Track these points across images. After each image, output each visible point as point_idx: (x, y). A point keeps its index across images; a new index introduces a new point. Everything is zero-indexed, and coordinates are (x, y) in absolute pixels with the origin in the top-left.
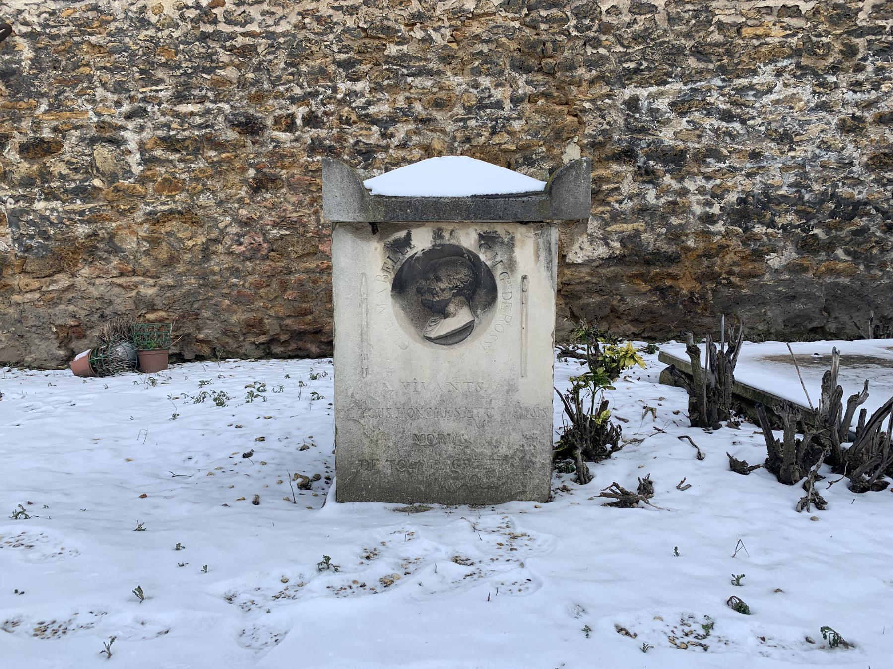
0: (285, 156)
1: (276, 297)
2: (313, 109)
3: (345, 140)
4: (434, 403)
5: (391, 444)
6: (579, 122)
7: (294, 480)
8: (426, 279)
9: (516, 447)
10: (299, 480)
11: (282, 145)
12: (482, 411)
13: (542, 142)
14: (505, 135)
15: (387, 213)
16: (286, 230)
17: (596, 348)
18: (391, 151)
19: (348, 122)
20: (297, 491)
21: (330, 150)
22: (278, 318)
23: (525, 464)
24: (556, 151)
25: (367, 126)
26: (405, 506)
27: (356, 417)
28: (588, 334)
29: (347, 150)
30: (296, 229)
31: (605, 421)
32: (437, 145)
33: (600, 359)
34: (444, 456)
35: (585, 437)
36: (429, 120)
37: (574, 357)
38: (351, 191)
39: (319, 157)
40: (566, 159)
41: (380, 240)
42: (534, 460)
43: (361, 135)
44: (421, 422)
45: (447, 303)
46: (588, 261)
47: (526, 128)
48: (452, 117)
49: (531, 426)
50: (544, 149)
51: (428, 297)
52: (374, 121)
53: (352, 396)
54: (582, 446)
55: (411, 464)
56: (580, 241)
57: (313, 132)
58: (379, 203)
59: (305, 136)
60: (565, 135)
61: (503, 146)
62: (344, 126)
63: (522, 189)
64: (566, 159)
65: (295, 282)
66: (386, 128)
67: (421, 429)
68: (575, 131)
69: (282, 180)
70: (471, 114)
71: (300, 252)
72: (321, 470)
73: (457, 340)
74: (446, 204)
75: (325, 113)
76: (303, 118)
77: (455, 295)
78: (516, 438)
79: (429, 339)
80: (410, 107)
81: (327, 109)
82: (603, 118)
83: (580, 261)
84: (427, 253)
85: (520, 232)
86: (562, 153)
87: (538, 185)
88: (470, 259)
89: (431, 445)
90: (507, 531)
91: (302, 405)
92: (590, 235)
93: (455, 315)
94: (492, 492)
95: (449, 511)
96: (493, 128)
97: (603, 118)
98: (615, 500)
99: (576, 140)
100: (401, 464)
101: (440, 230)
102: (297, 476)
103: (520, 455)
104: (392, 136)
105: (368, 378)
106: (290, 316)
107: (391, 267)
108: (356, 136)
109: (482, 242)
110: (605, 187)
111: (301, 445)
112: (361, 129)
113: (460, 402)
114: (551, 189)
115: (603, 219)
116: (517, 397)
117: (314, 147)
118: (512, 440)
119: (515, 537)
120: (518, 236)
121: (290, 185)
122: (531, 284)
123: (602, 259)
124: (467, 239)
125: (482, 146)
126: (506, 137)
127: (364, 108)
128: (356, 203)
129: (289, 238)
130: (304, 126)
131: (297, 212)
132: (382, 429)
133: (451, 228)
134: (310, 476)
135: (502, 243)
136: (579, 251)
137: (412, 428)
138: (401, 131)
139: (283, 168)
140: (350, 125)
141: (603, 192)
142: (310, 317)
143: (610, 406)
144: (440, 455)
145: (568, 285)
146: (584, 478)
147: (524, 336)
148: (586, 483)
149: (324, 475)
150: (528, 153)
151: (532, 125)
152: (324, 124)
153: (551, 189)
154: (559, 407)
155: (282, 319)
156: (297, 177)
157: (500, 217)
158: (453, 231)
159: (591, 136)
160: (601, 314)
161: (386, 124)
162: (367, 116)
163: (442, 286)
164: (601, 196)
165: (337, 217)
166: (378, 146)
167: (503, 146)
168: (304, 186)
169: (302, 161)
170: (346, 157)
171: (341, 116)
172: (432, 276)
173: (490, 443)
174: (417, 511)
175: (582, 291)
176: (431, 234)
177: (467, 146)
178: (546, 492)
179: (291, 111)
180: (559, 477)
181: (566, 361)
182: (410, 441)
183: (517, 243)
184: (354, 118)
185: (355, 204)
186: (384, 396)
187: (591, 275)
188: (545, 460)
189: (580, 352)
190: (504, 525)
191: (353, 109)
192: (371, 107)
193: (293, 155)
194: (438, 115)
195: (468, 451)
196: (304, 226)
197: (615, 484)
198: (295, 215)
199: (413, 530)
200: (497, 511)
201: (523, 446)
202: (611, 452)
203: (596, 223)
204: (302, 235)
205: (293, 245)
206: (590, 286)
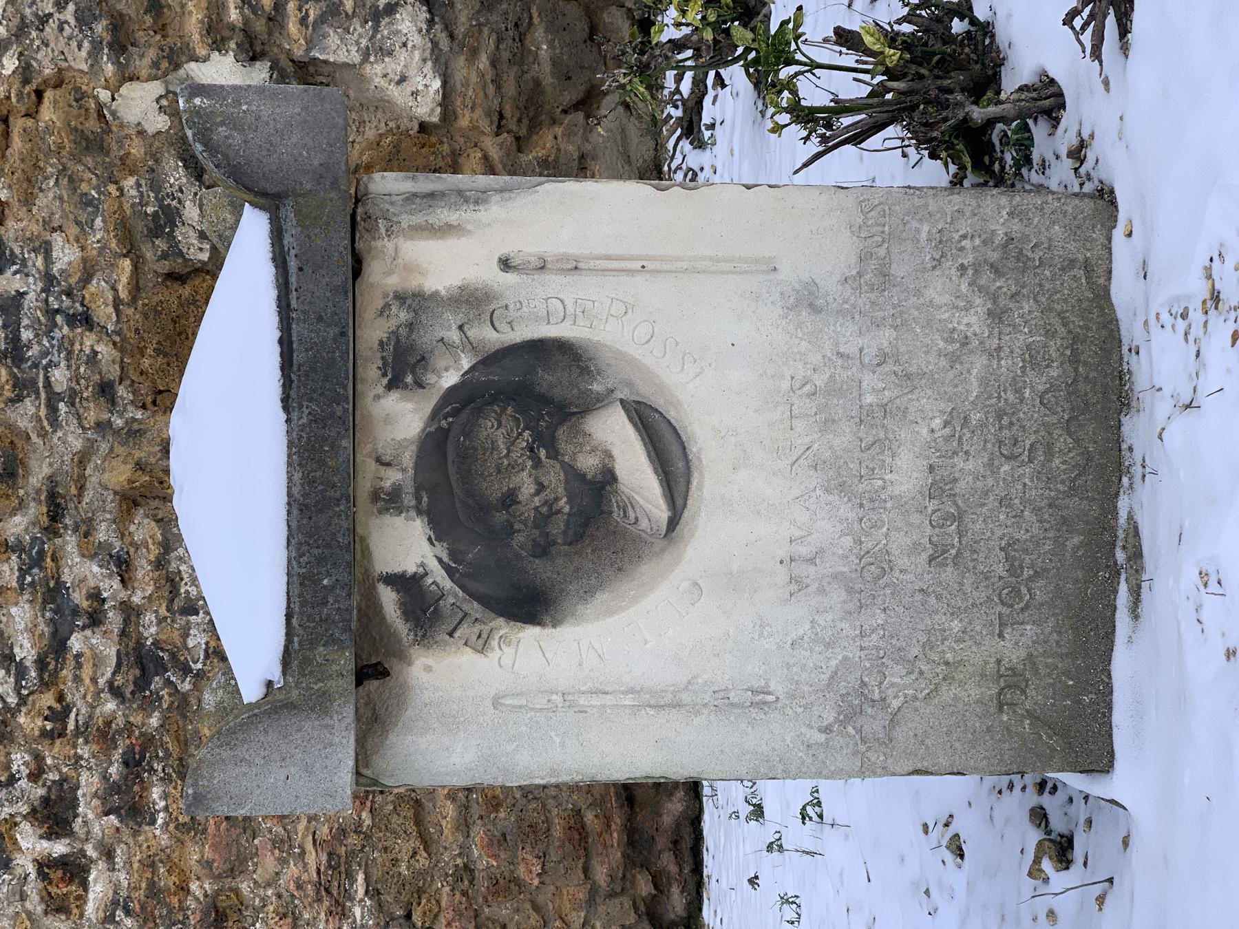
0: (152, 884)
1: (536, 907)
2: (25, 809)
3: (108, 724)
4: (846, 511)
5: (956, 625)
6: (57, 86)
7: (1046, 880)
8: (510, 530)
9: (964, 288)
10: (1047, 865)
11: (124, 893)
12: (868, 380)
13: (112, 188)
14: (93, 287)
15: (332, 640)
16: (351, 878)
17: (677, 45)
18: (137, 599)
19: (59, 715)
20: (1073, 876)
21: (133, 763)
22: (591, 901)
23: (1011, 263)
24: (137, 149)
25: (71, 663)
26: (1123, 588)
27: (882, 720)
28: (642, 70)
29: (136, 719)
30: (351, 854)
31: (892, 39)
32: (120, 475)
33: (708, 35)
34: (990, 481)
35: (933, 93)
36: (52, 496)
37: (699, 104)
38: (272, 737)
39: (156, 793)
40: (159, 123)
41: (402, 656)
42: (1000, 237)
43: (94, 680)
44: (899, 542)
45: (574, 476)
46: (436, 61)
47: (73, 230)
48: (43, 434)
49: (909, 246)
50: (129, 182)
51: (557, 528)
52: (58, 645)
53: (827, 730)
54: (959, 105)
55: (1011, 571)
56: (383, 83)
57: (87, 809)
58: (306, 661)
59: (96, 829)
60: (92, 125)
61: (123, 294)
62: (71, 726)
63: (267, 271)
64: (159, 123)
65: (496, 857)
66: (76, 612)
67: (916, 544)
68: (80, 96)
69: (217, 893)
70: (34, 382)
71: (414, 843)
72: (1018, 804)
73: (674, 448)
74: (309, 481)
75: (34, 777)
76: (50, 836)
77: (554, 454)
78: (940, 289)
79: (673, 523)
80: (18, 548)
81: (25, 771)
82: (44, 19)
83: (437, 84)
84: (440, 529)
85: (382, 277)
86: (141, 133)
87: (253, 229)
88: (455, 413)
89: (959, 518)
90: (1196, 316)
91: (831, 842)
92: (366, 54)
93: (608, 454)
94: (1088, 353)
95: (1137, 470)
96: (72, 320)
97: (44, 19)
98: (1111, 22)
99: (104, 95)
100: (1011, 598)
101: (375, 496)
102: (1035, 872)
103: (986, 277)
104: (95, 596)
105: (778, 687)
106: (586, 870)
107: (477, 628)
108: (98, 693)
109: (409, 379)
110: (234, 15)
111: (949, 857)
112: (77, 679)
113: (844, 438)
114: (264, 194)
115: (321, 20)
116: (830, 285)
117: (128, 805)
118: (946, 298)
119: (1216, 297)
120: (393, 282)
121: (232, 872)
122: (525, 245)
123: (431, 23)
124: (400, 420)
125: (122, 350)
126: (98, 285)
127: (21, 672)
128: (307, 725)
129: (376, 873)
130: (70, 834)
131: (303, 853)
132: (915, 651)
133: (372, 465)
134: (1033, 836)
135: (411, 326)
136: (408, 88)
137: (912, 569)
138: (82, 572)
139: (184, 889)
140: (67, 710)
141: (246, 21)
142: (589, 817)
143: (853, 24)
144: (986, 494)
145: (501, 117)
146: (1047, 99)
147: (666, 267)
148: (1061, 95)
149: (1032, 799)
150: (140, 227)
151: (65, 216)
152: (64, 779)
153: (264, 194)
154: (847, 164)
155: (593, 892)
156: (208, 853)
157: (343, 334)
158: (379, 461)
159: (94, 54)
160: (581, 29)
161: (63, 613)
162: (41, 663)
163: (528, 488)
164: (260, 26)
165: (345, 778)
166: (123, 634)
167: (123, 294)
168: (235, 832)
169: (164, 840)
170: (154, 721)
171: (44, 734)
172: (500, 517)
173: (954, 359)
174: (1136, 555)
175: (518, 79)
176: (388, 519)
177: (122, 391)
178: (1088, 206)
179: (31, 869)
180: (1044, 166)
181: (712, 127)
182: (949, 574)
183: (413, 283)
184: (47, 700)
185: (309, 726)
186: (828, 645)
187: (474, 53)
188: (1000, 208)
189: (686, 87)
190: (1181, 325)
191: (23, 701)
192: (19, 654)
193: (150, 864)
194: (38, 473)
195: (976, 417)
196: (343, 832)
197: (1068, 20)
198: (311, 859)
199: (1190, 575)
200: (1139, 340)
201: (963, 268)
202: (974, 21)
203: (333, 40)
204: (368, 837)
205: (395, 862)
206: (506, 55)
